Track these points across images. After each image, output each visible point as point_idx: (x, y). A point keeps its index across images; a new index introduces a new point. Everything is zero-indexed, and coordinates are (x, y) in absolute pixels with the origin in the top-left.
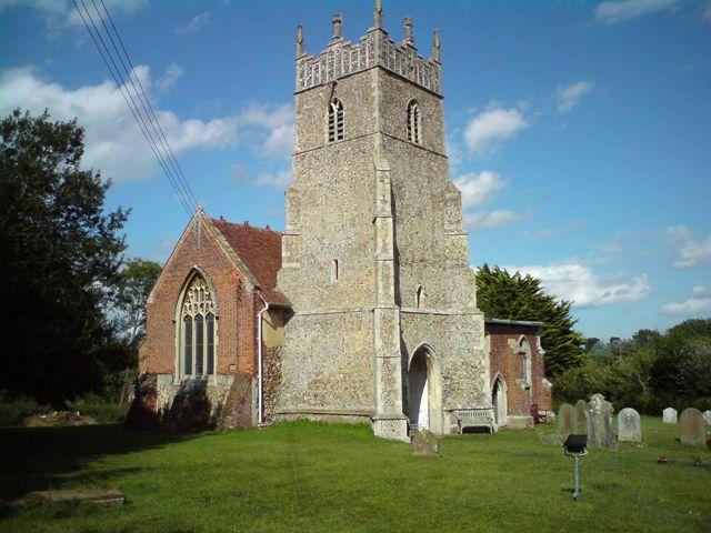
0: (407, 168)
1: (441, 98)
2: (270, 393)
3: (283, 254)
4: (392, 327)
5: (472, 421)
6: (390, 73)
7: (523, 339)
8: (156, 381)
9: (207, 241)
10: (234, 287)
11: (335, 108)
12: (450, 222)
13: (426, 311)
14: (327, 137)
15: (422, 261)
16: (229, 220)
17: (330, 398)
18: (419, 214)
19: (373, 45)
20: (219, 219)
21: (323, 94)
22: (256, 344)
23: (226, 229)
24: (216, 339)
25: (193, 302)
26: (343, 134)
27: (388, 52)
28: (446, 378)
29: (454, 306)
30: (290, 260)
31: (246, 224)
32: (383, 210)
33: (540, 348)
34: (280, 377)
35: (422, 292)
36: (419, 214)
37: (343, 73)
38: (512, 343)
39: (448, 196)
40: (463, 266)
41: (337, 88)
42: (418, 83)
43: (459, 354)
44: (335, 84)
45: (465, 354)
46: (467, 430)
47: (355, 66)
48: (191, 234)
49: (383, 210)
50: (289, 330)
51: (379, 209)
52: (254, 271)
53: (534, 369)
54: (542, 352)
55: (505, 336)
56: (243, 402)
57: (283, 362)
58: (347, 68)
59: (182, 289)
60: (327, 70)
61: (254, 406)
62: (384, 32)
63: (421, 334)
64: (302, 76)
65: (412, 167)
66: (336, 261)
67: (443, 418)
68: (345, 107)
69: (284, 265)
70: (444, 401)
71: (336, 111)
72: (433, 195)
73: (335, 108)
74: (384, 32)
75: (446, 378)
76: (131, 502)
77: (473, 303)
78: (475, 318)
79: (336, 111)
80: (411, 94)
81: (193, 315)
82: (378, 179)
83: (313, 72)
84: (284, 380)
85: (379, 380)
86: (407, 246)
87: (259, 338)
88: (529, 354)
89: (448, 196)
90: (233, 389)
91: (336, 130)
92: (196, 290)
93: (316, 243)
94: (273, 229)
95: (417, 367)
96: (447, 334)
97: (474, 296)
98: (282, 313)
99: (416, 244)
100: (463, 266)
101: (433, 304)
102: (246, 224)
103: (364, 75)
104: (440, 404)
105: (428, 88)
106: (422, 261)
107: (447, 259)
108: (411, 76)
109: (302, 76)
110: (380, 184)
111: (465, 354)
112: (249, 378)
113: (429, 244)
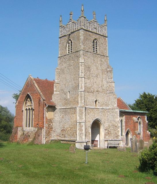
0: (92, 61)
1: (107, 37)
2: (48, 134)
3: (54, 89)
4: (82, 113)
5: (113, 143)
6: (86, 30)
7: (139, 117)
8: (18, 129)
9: (32, 85)
10: (38, 100)
11: (70, 42)
12: (109, 78)
13: (98, 108)
14: (68, 52)
15: (97, 91)
16: (40, 78)
17: (66, 135)
18: (97, 76)
19: (80, 22)
20: (37, 78)
21: (66, 38)
22: (44, 118)
23: (38, 81)
24: (33, 116)
25: (28, 104)
26: (72, 51)
27: (85, 23)
28: (106, 130)
29: (109, 106)
30: (56, 91)
31: (46, 79)
32: (81, 75)
33: (146, 120)
34: (52, 128)
35: (97, 102)
36: (97, 76)
37: (72, 31)
38: (135, 119)
39: (108, 70)
40: (113, 93)
41: (70, 36)
42: (98, 33)
43: (111, 122)
44: (70, 35)
45: (113, 122)
46: (110, 147)
47: (76, 29)
48: (28, 83)
49: (81, 75)
50: (56, 113)
51: (80, 75)
52: (45, 95)
53: (143, 127)
54: (147, 122)
55: (131, 116)
56: (39, 136)
57: (53, 124)
58: (73, 30)
59: (25, 100)
60: (68, 30)
61: (43, 137)
62: (84, 17)
63: (96, 116)
64: (61, 32)
65: (94, 61)
66: (69, 92)
67: (105, 143)
68: (73, 42)
69: (55, 93)
70: (105, 137)
71: (70, 43)
72: (102, 70)
73: (70, 42)
74: (84, 17)
75: (106, 130)
76: (63, 179)
77: (116, 105)
78: (116, 110)
79: (70, 43)
80: (94, 36)
81: (28, 108)
82: (80, 65)
83: (64, 31)
84: (53, 129)
85: (78, 129)
86: (91, 87)
87: (45, 116)
88: (142, 123)
89: (108, 70)
90: (37, 132)
91: (70, 48)
92: (29, 101)
93: (64, 85)
94: (48, 79)
95: (96, 125)
96: (107, 115)
97: (116, 103)
98: (52, 108)
99: (95, 86)
100: (113, 93)
101: (102, 105)
102: (46, 79)
103: (78, 32)
104: (103, 138)
105: (102, 34)
106: (97, 91)
107: (107, 90)
108: (95, 31)
109: (61, 32)
110: (81, 67)
111: (113, 122)
112: (41, 128)
113: (100, 86)
